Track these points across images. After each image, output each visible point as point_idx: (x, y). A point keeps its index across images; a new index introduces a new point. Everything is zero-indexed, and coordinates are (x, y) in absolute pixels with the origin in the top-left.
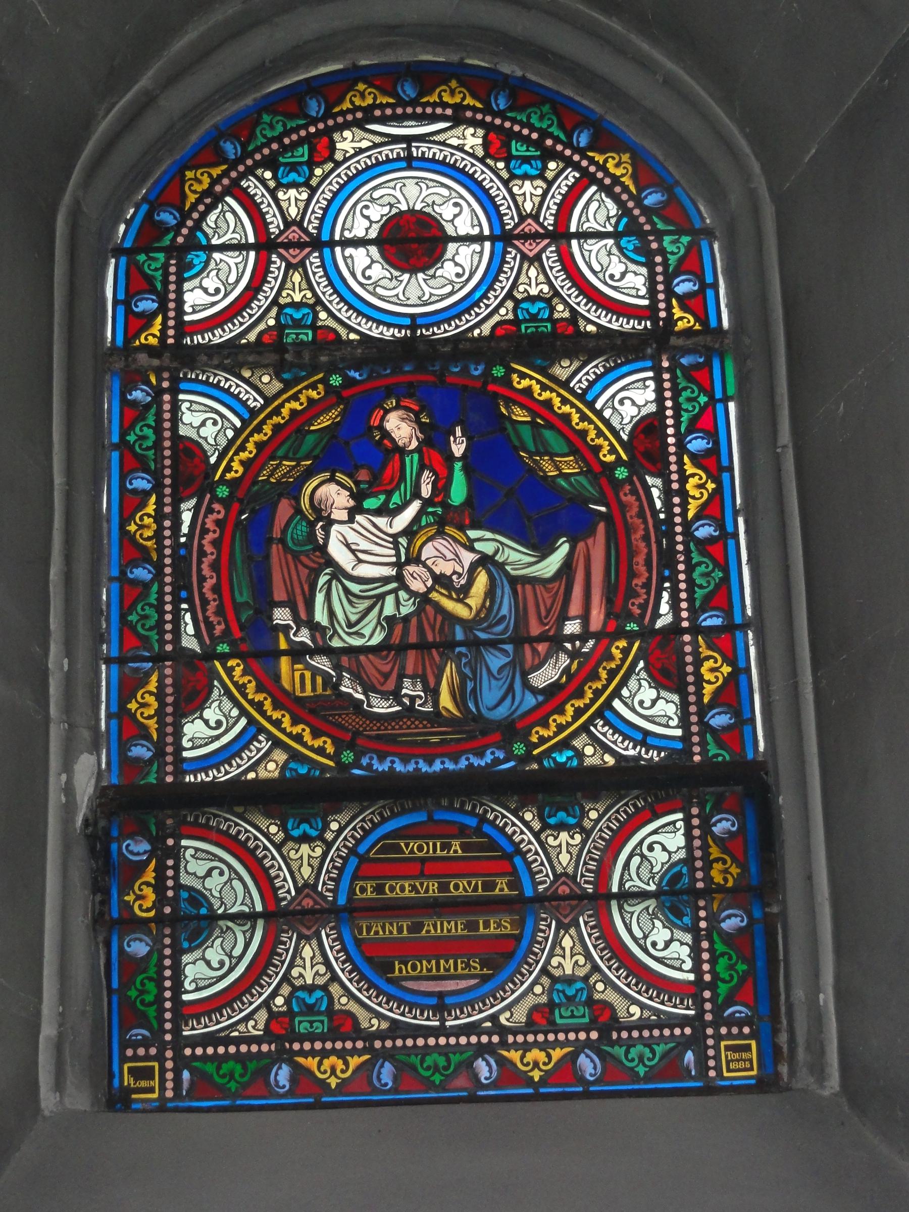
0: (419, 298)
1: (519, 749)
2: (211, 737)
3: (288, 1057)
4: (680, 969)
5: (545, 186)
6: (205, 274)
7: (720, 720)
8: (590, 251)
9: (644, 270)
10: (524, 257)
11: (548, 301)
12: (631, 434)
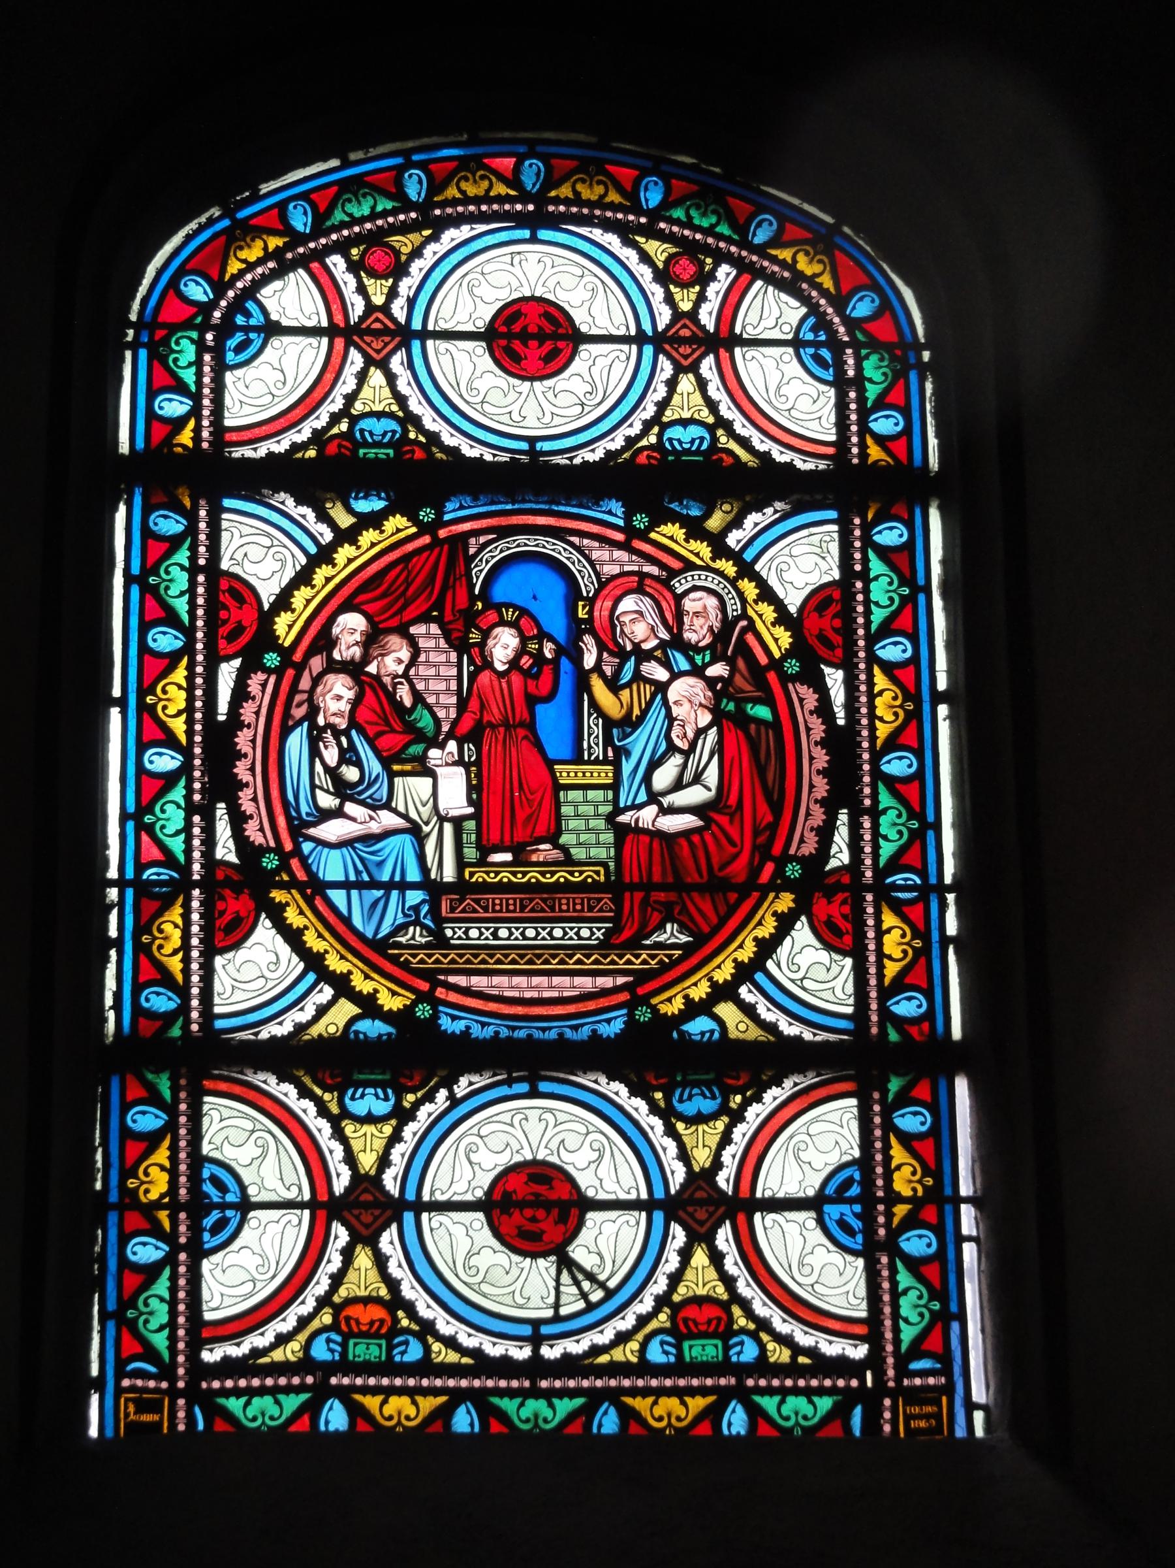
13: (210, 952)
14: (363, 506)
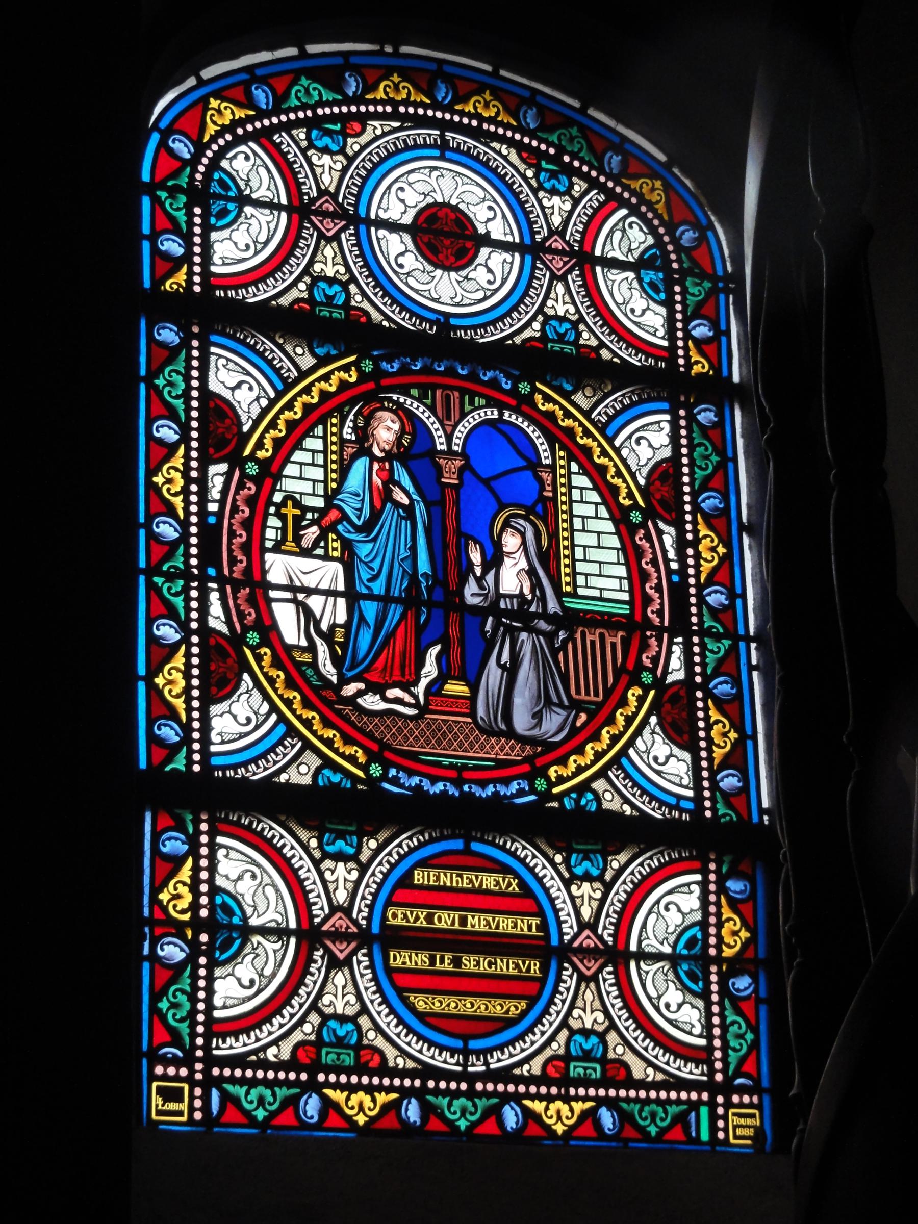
0: (452, 298)
1: (541, 784)
2: (240, 734)
3: (313, 1087)
4: (690, 1033)
5: (345, 163)
6: (235, 227)
7: (729, 781)
8: (614, 281)
9: (663, 311)
10: (321, 236)
11: (345, 286)
12: (648, 478)
13: (207, 701)
14: (320, 351)
